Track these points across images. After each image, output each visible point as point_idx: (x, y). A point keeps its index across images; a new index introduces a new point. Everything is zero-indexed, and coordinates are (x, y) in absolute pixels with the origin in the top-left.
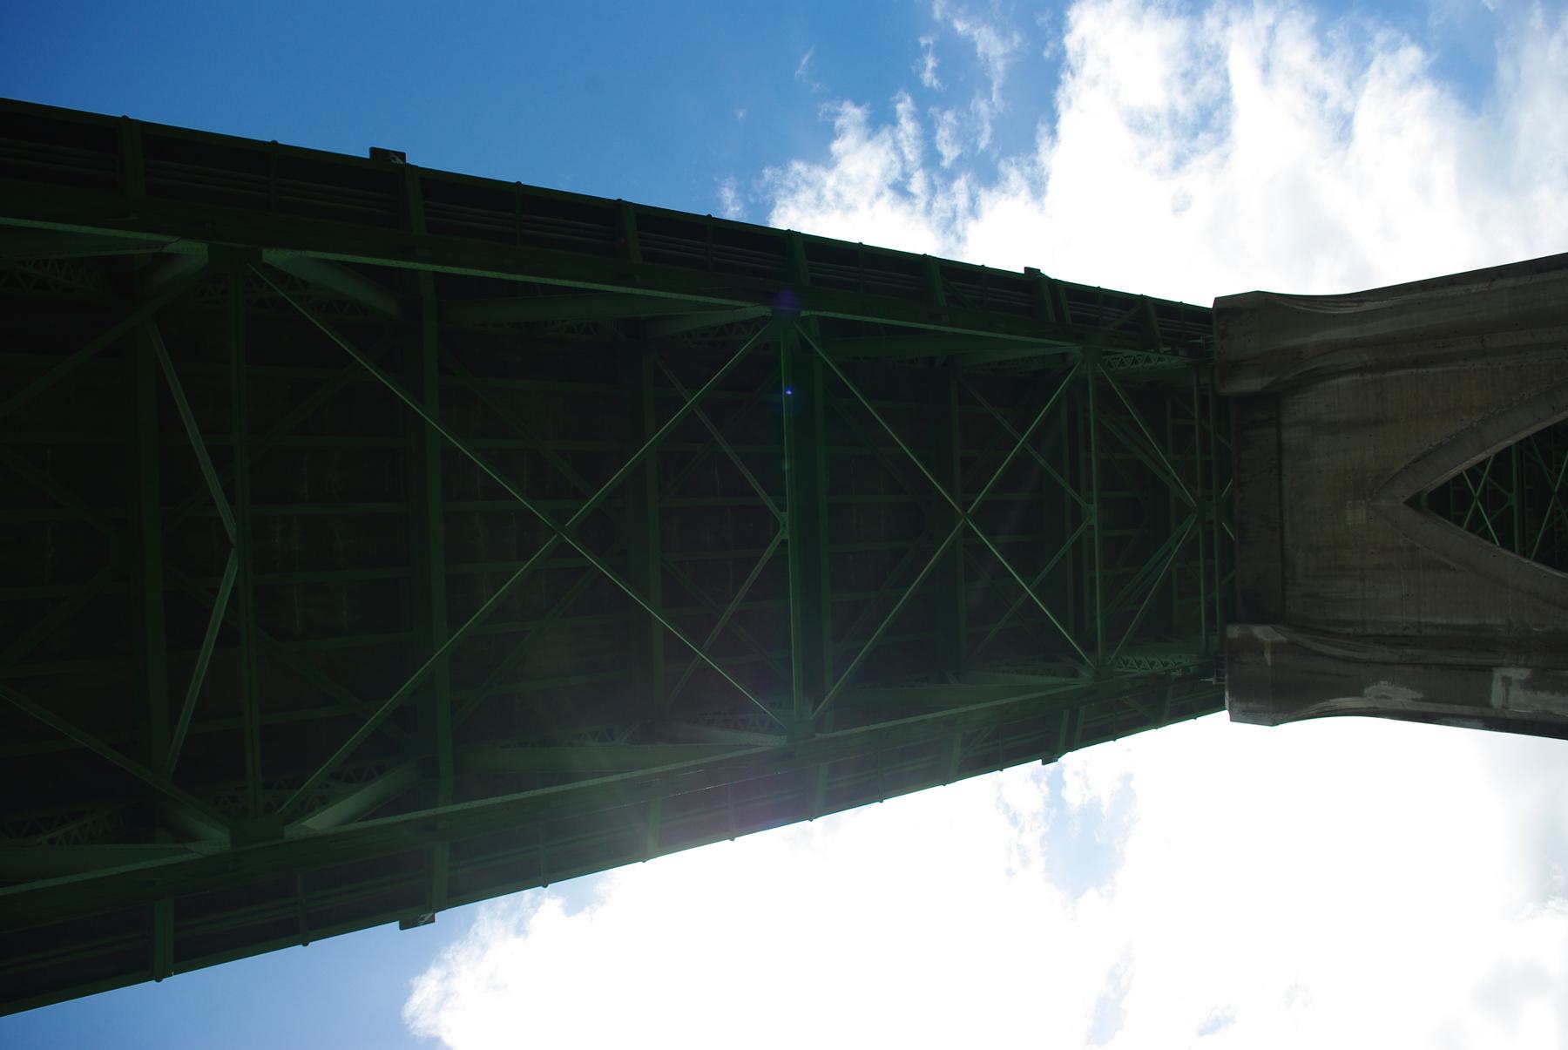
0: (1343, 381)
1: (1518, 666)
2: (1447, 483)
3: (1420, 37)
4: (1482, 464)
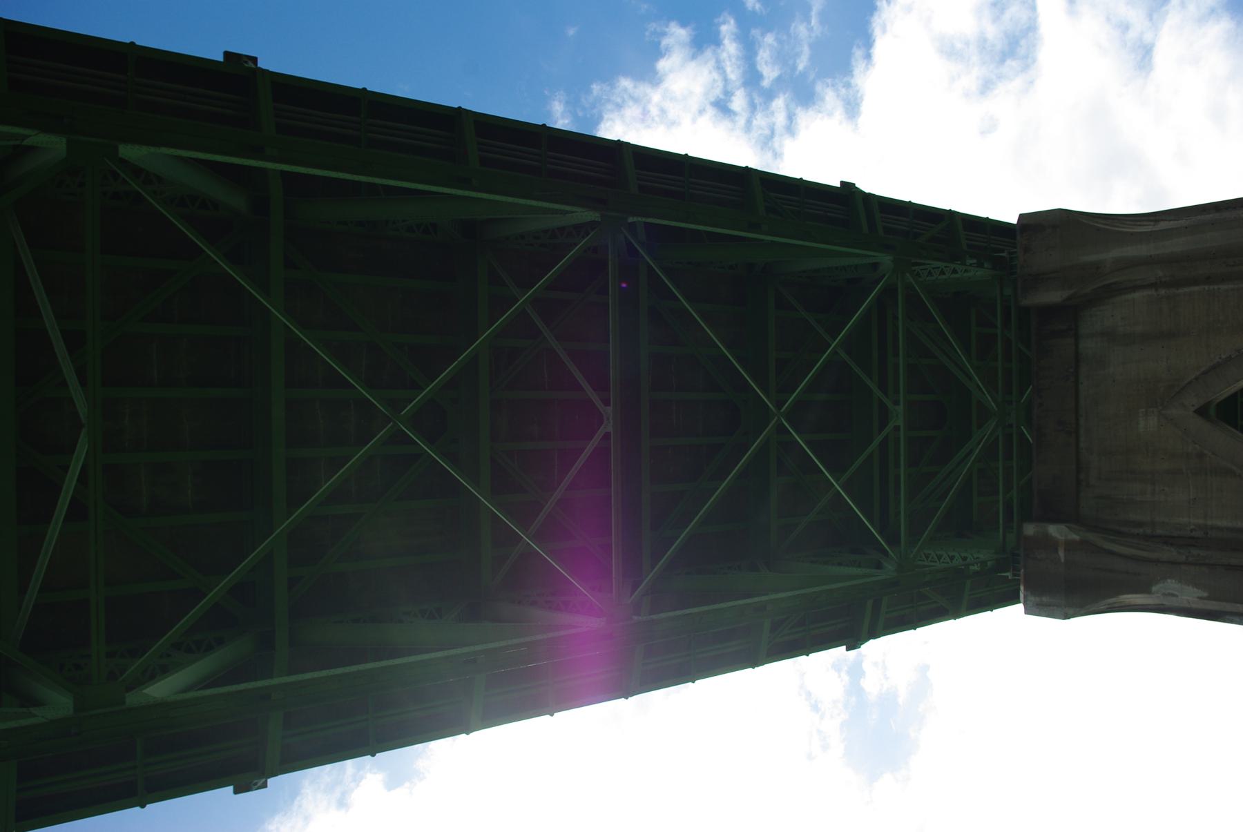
0: (1137, 295)
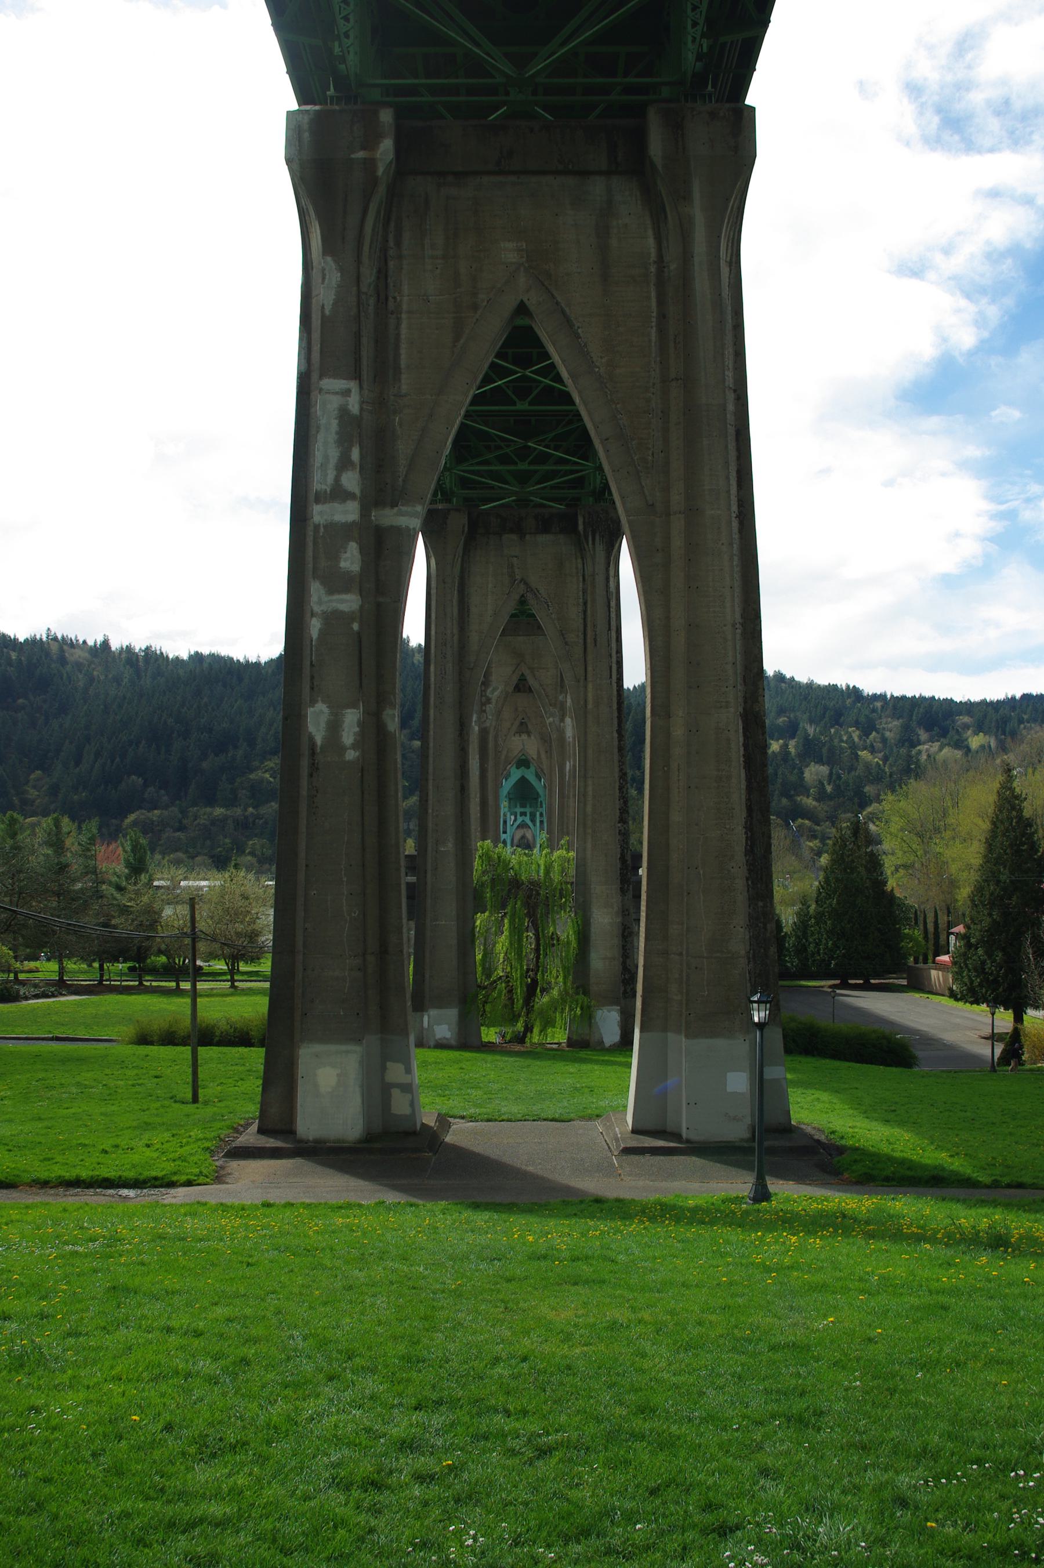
0: (651, 242)
1: (362, 403)
2: (543, 347)
3: (984, 348)
4: (558, 379)
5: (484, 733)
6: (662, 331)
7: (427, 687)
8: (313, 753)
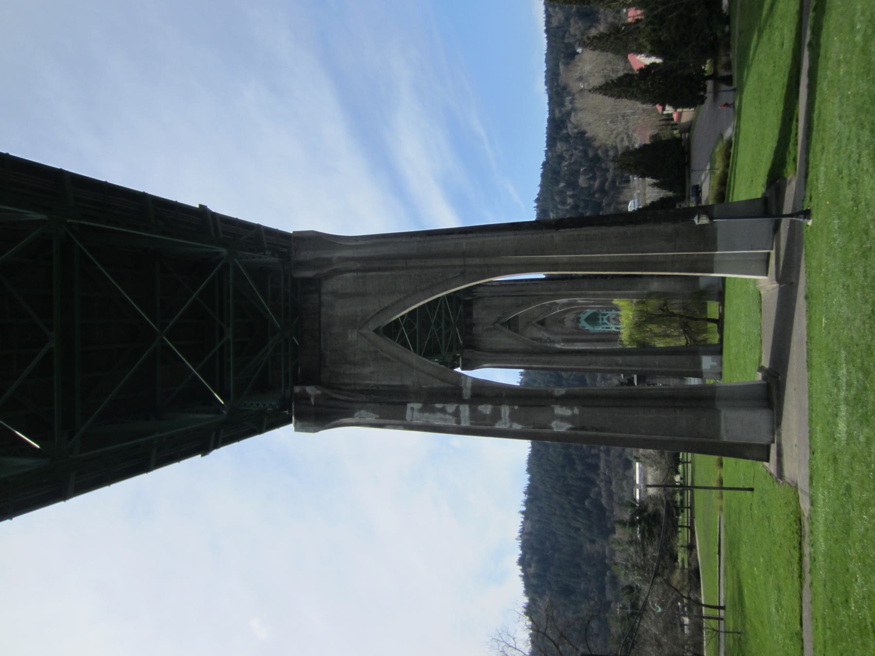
0: (348, 275)
5: (566, 341)
6: (386, 269)
7: (543, 369)
8: (575, 429)
